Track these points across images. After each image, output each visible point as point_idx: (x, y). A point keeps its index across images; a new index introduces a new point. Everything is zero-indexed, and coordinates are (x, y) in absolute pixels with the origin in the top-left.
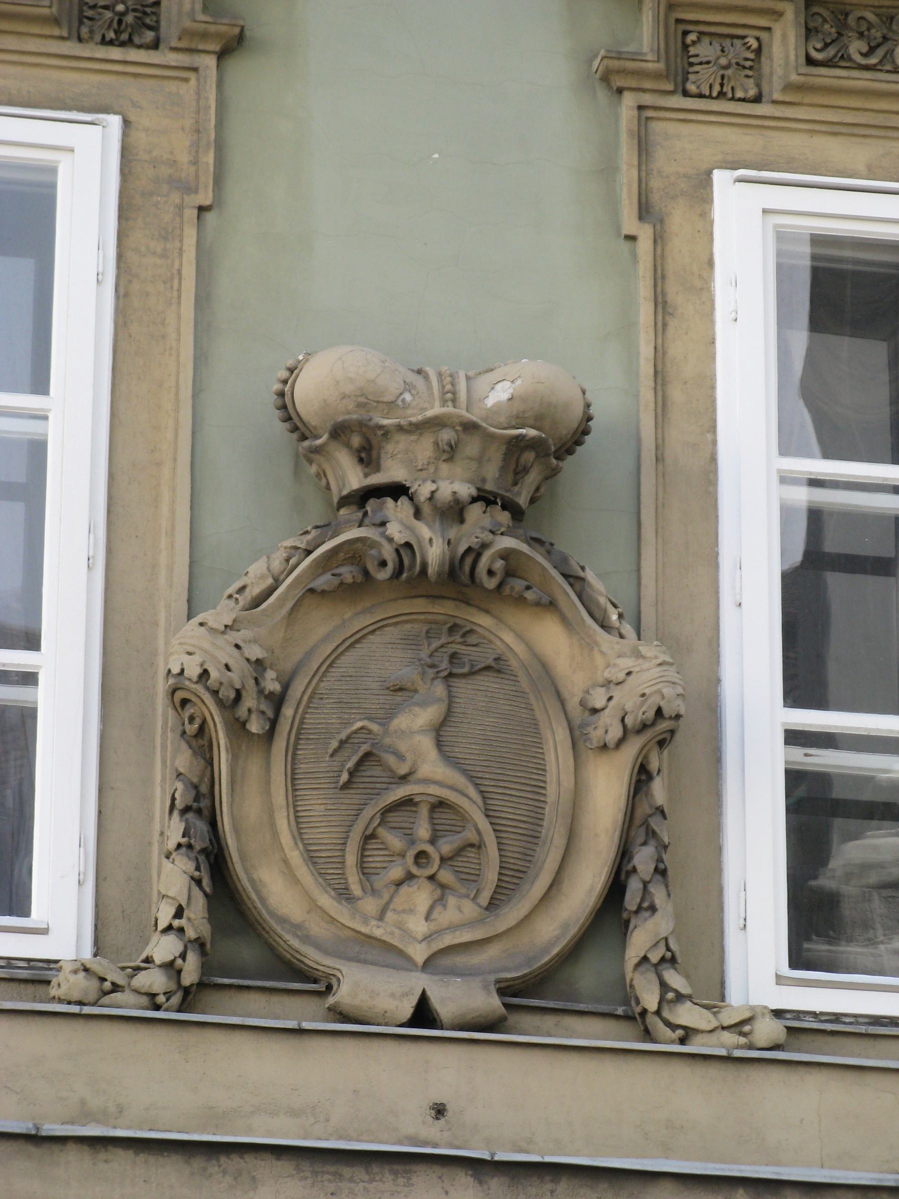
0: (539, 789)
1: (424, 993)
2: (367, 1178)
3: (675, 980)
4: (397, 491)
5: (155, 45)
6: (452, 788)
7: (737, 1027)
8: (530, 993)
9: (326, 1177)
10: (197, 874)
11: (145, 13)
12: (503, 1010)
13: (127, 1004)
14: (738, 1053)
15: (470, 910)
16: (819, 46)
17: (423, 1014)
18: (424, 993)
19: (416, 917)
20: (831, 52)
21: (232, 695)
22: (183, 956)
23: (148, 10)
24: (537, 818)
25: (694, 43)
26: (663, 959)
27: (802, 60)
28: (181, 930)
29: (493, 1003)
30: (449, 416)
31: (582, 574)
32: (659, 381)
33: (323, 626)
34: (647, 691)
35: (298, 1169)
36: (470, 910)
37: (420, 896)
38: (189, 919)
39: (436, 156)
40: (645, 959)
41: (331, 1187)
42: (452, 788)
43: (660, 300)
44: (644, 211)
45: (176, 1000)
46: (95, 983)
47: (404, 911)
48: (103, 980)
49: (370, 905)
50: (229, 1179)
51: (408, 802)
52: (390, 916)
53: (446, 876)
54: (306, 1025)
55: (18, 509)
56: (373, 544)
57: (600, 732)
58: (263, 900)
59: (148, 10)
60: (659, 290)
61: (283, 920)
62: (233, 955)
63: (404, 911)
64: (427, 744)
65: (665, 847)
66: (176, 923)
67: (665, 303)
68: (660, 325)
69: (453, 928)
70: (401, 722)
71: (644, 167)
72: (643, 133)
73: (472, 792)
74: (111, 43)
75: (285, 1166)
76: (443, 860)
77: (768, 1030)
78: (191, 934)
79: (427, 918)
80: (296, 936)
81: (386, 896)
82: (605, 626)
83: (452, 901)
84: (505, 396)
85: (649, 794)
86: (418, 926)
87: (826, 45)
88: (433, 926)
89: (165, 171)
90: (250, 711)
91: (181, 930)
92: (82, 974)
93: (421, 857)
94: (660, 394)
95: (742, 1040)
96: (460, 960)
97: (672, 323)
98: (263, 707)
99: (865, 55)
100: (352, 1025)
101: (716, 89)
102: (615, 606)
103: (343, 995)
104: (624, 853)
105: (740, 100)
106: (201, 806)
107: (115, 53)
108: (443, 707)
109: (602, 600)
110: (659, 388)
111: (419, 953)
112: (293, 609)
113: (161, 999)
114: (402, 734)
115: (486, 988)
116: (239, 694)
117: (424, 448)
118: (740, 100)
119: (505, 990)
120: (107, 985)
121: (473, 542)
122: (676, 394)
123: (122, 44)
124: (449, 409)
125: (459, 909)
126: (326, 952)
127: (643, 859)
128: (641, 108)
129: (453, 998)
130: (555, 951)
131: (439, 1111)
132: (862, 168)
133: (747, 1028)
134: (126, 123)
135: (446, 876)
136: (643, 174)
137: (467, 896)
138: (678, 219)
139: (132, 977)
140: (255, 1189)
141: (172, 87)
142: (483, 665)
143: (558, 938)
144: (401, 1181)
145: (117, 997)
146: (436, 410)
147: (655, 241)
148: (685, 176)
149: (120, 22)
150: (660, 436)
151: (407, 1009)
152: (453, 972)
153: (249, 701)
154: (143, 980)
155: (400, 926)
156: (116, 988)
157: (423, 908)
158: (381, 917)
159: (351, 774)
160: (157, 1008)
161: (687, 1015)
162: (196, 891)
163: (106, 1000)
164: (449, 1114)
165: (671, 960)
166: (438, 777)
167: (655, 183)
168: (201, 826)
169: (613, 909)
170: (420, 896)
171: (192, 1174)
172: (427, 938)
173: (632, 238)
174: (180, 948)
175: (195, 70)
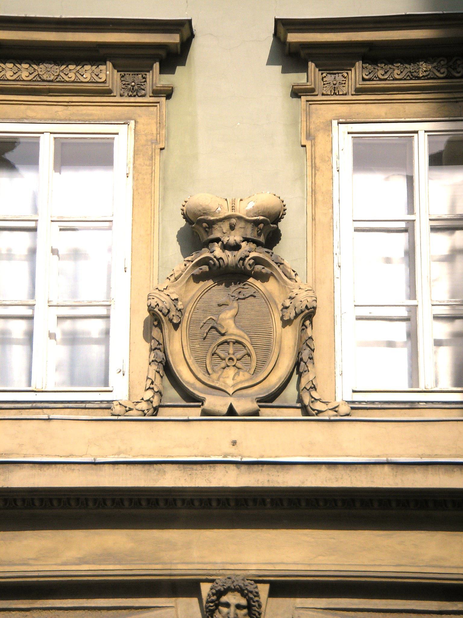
0: (270, 334)
1: (231, 404)
2: (201, 469)
3: (314, 394)
4: (218, 240)
5: (144, 96)
6: (239, 336)
7: (334, 409)
8: (269, 399)
9: (188, 469)
10: (158, 370)
11: (141, 85)
12: (258, 407)
13: (134, 415)
14: (332, 418)
16: (367, 74)
17: (231, 411)
18: (231, 404)
19: (229, 379)
20: (371, 75)
21: (167, 311)
22: (153, 397)
23: (143, 84)
25: (325, 77)
26: (311, 388)
27: (361, 79)
28: (153, 389)
29: (255, 406)
30: (233, 215)
31: (282, 262)
32: (313, 193)
34: (302, 300)
35: (179, 467)
36: (247, 376)
38: (156, 385)
39: (239, 124)
40: (305, 388)
41: (190, 472)
42: (239, 336)
43: (314, 165)
44: (309, 136)
45: (151, 411)
46: (124, 408)
47: (225, 377)
48: (126, 407)
50: (157, 472)
51: (227, 342)
52: (221, 379)
53: (239, 364)
54: (191, 418)
56: (211, 259)
57: (288, 314)
58: (181, 377)
59: (143, 84)
60: (313, 162)
61: (188, 383)
63: (225, 377)
64: (231, 323)
65: (313, 350)
66: (152, 386)
67: (315, 166)
68: (313, 175)
69: (241, 382)
70: (222, 316)
71: (308, 121)
72: (308, 110)
73: (246, 337)
74: (131, 96)
75: (175, 466)
76: (238, 360)
77: (344, 409)
78: (156, 390)
79: (233, 379)
80: (192, 387)
81: (220, 373)
82: (290, 279)
83: (241, 373)
84: (251, 207)
85: (306, 333)
87: (370, 73)
88: (235, 382)
89: (149, 137)
90: (173, 316)
91: (153, 389)
92: (119, 406)
93: (231, 359)
94: (314, 197)
95: (336, 413)
96: (244, 392)
97: (318, 174)
98: (177, 314)
99: (383, 75)
101: (333, 92)
102: (294, 271)
103: (206, 405)
105: (341, 95)
107: (132, 99)
108: (236, 310)
109: (289, 270)
110: (313, 195)
111: (231, 391)
112: (187, 281)
113: (146, 411)
114: (223, 320)
115: (252, 401)
116: (169, 311)
117: (225, 227)
118: (341, 95)
120: (127, 409)
121: (243, 256)
122: (319, 197)
123: (135, 96)
124: (233, 213)
125: (244, 375)
126: (202, 392)
127: (305, 355)
128: (307, 101)
129: (240, 406)
130: (277, 387)
131: (234, 443)
132: (383, 114)
133: (337, 409)
134: (136, 122)
136: (308, 124)
137: (246, 371)
138: (321, 138)
139: (136, 405)
140: (165, 474)
141: (151, 109)
142: (249, 295)
143: (277, 383)
144: (212, 469)
145: (130, 412)
146: (230, 213)
147: (312, 146)
148: (323, 122)
149: (133, 89)
150: (314, 212)
151: (225, 410)
152: (242, 396)
153: (173, 313)
154: (139, 406)
155: (224, 382)
156: (130, 409)
157: (232, 376)
158: (218, 379)
159: (207, 334)
160: (145, 415)
161: (318, 406)
162: (157, 375)
163: (127, 414)
164: (237, 444)
165: (314, 388)
166: (235, 333)
167: (312, 126)
168: (161, 354)
169: (298, 367)
170: (231, 372)
171: (145, 471)
172: (233, 386)
173: (304, 146)
174: (152, 394)
175: (158, 103)
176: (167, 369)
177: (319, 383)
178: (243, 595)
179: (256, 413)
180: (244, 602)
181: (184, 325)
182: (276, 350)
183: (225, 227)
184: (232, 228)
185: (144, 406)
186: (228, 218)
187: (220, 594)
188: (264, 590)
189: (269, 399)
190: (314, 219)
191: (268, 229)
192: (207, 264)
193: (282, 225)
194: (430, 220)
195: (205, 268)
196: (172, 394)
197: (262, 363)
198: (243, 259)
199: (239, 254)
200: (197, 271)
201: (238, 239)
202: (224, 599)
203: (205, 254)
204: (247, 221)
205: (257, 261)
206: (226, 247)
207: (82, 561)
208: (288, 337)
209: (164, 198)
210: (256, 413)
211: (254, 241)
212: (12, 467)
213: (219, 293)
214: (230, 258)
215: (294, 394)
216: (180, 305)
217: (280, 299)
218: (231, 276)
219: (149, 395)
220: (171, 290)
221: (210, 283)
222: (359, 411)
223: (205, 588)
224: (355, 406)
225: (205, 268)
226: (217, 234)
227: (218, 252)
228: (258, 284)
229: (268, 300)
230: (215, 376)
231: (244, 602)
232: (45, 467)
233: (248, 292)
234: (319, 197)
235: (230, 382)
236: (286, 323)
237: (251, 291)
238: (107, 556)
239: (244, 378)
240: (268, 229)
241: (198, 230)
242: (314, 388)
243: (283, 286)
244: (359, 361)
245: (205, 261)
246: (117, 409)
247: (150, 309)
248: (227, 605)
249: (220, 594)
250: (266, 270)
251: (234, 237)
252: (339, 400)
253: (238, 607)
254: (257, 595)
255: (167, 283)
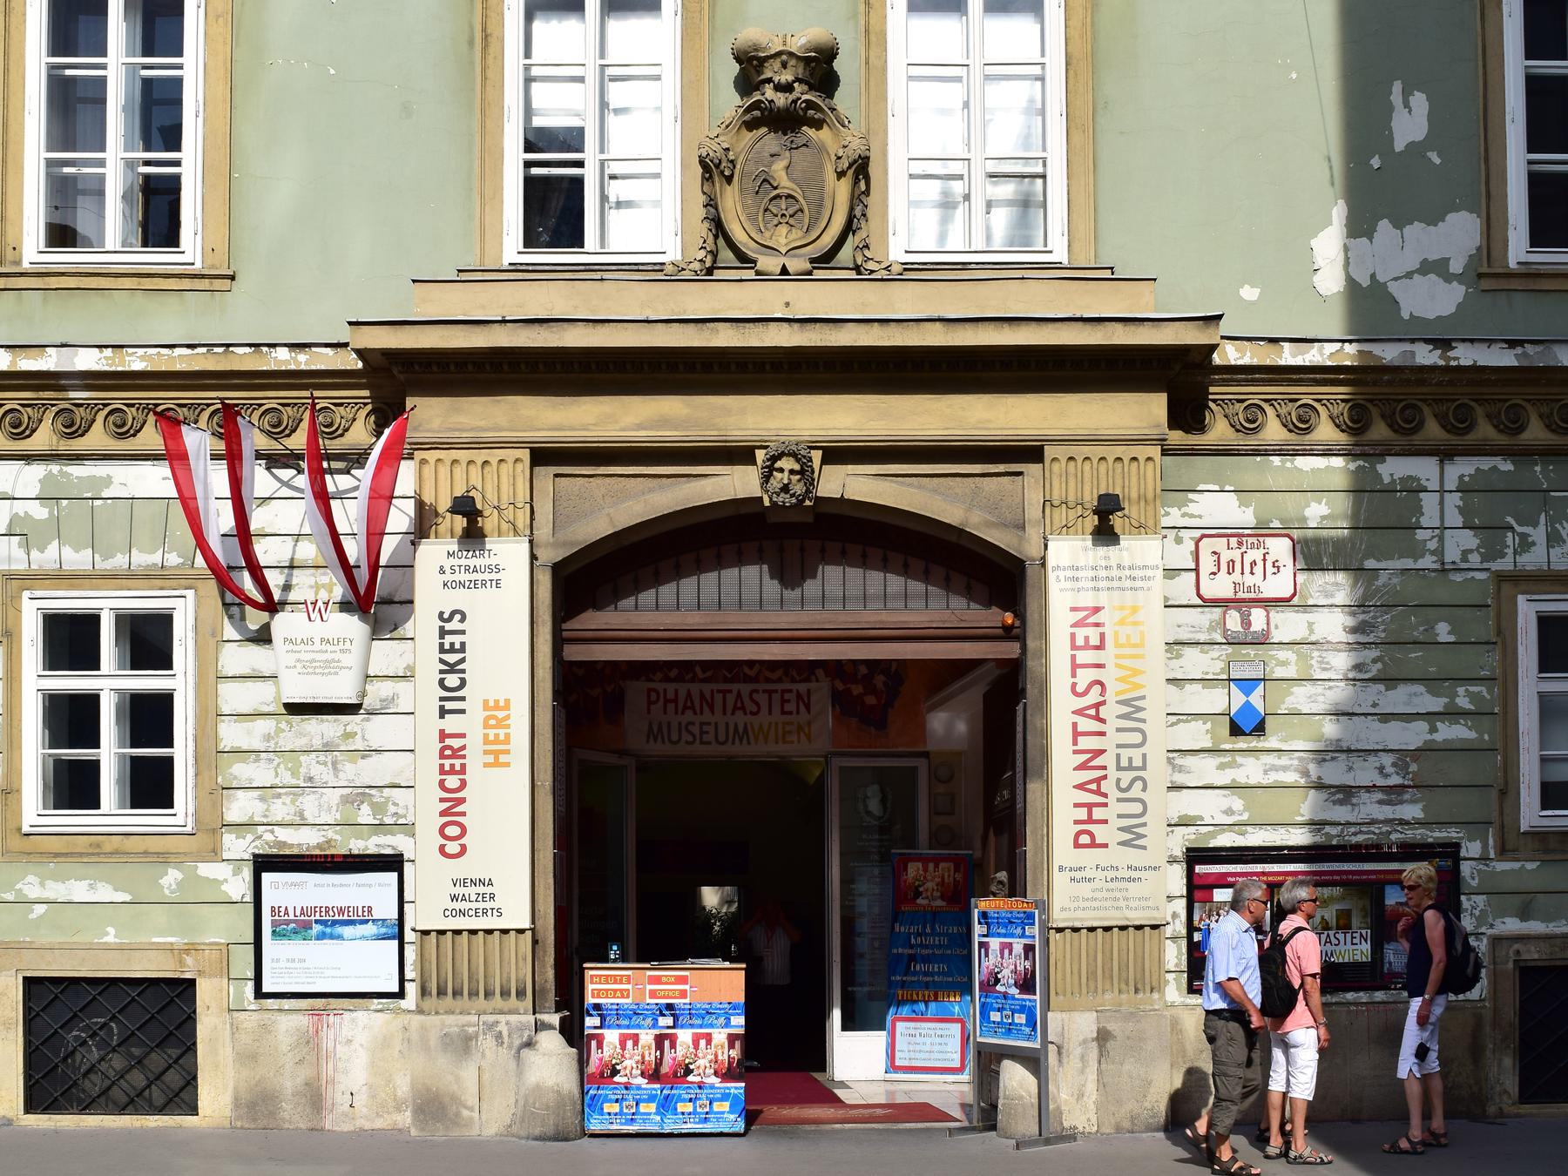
0: (822, 188)
4: (769, 80)
8: (826, 259)
13: (687, 275)
15: (800, 234)
17: (784, 271)
19: (782, 237)
24: (822, 199)
29: (808, 266)
33: (748, 137)
36: (800, 234)
37: (784, 229)
39: (1294, 76)
49: (767, 234)
51: (778, 197)
53: (792, 221)
55: (1039, 83)
62: (722, 252)
64: (783, 173)
86: (783, 241)
100: (763, 277)
104: (852, 209)
106: (711, 203)
117: (777, 64)
119: (812, 261)
122: (873, 38)
127: (858, 212)
129: (794, 265)
131: (787, 304)
135: (792, 221)
161: (871, 265)
165: (867, 247)
169: (849, 228)
170: (784, 229)
176: (718, 227)
177: (872, 242)
178: (798, 460)
179: (810, 273)
180: (797, 467)
181: (736, 178)
182: (828, 204)
183: (777, 64)
184: (784, 65)
185: (697, 266)
186: (779, 54)
187: (774, 459)
188: (817, 456)
189: (826, 259)
190: (867, 63)
191: (820, 68)
192: (759, 108)
193: (836, 65)
194: (463, 711)
195: (757, 113)
196: (727, 255)
197: (813, 221)
198: (794, 102)
199: (791, 97)
200: (747, 117)
201: (790, 78)
202: (778, 464)
203: (757, 97)
204: (799, 58)
205: (810, 105)
206: (780, 88)
207: (640, 427)
208: (843, 189)
209: (711, 39)
210: (810, 273)
211: (807, 83)
212: (566, 325)
213: (771, 141)
214: (781, 100)
215: (842, 251)
216: (731, 156)
217: (833, 148)
218: (786, 122)
219: (702, 254)
220: (721, 138)
221: (764, 130)
222: (912, 272)
223: (760, 455)
224: (908, 267)
225: (757, 113)
226: (768, 74)
227: (769, 92)
228: (811, 132)
229: (821, 149)
230: (767, 234)
231: (797, 467)
232: (600, 326)
233: (800, 141)
234: (874, 38)
235: (783, 241)
236: (841, 175)
237: (800, 141)
238: (663, 422)
239: (797, 237)
240: (820, 68)
241: (751, 67)
242: (867, 247)
243: (837, 134)
244: (909, 225)
245: (756, 105)
246: (669, 269)
247: (702, 162)
248: (781, 470)
249: (774, 459)
250: (818, 116)
251: (786, 77)
252: (892, 258)
253: (792, 472)
254: (811, 460)
255: (718, 131)
